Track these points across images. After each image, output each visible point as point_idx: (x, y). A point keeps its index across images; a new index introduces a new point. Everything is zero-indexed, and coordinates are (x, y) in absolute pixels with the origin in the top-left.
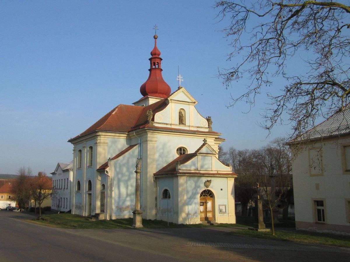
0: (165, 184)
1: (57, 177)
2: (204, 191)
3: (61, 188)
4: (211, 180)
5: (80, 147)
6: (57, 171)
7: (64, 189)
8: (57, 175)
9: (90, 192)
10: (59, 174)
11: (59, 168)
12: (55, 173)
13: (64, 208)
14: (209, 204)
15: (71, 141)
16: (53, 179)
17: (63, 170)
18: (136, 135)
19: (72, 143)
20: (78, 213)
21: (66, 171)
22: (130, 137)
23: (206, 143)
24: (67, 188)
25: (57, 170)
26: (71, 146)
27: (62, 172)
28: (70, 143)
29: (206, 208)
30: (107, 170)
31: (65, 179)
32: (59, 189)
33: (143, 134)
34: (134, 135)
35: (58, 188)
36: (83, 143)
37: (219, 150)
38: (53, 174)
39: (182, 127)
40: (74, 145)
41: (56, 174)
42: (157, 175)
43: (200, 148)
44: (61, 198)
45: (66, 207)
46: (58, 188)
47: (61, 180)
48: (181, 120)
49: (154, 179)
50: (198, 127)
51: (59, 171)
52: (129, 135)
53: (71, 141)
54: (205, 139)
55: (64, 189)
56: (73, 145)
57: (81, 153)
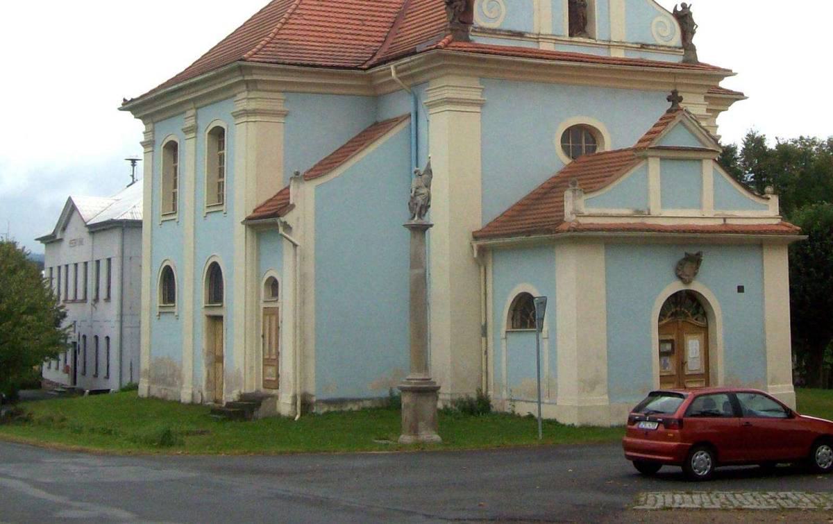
0: (514, 278)
1: (68, 254)
2: (675, 299)
3: (80, 296)
4: (699, 254)
5: (172, 130)
6: (64, 229)
7: (97, 299)
8: (66, 243)
9: (216, 312)
10: (74, 243)
11: (75, 218)
12: (58, 237)
13: (96, 376)
14: (693, 346)
15: (133, 106)
16: (47, 265)
17: (88, 224)
18: (399, 78)
19: (137, 116)
20: (156, 391)
21: (100, 231)
22: (375, 88)
23: (680, 109)
24: (108, 299)
25: (63, 224)
26: (135, 128)
27: (84, 233)
28: (129, 113)
29: (682, 364)
30: (285, 223)
31: (98, 262)
32: (75, 301)
33: (427, 76)
34: (393, 81)
35: (71, 297)
36: (184, 113)
37: (671, 94)
38: (50, 240)
39: (580, 47)
40: (145, 124)
41: (61, 240)
42: (483, 237)
43: (159, 87)
44: (84, 337)
45: (103, 373)
46: (71, 297)
47: (72, 268)
48: (706, 119)
49: (475, 255)
50: (644, 46)
51: (75, 231)
52: (371, 81)
53: (133, 106)
54: (675, 93)
55: (97, 299)
56: (140, 121)
57: (175, 160)
